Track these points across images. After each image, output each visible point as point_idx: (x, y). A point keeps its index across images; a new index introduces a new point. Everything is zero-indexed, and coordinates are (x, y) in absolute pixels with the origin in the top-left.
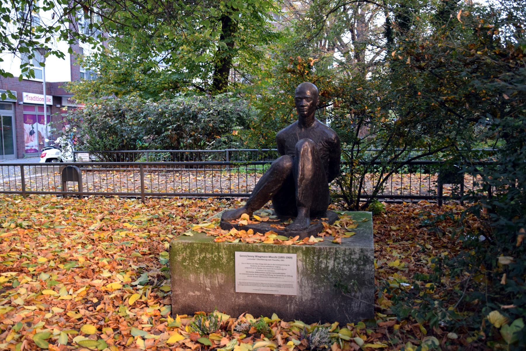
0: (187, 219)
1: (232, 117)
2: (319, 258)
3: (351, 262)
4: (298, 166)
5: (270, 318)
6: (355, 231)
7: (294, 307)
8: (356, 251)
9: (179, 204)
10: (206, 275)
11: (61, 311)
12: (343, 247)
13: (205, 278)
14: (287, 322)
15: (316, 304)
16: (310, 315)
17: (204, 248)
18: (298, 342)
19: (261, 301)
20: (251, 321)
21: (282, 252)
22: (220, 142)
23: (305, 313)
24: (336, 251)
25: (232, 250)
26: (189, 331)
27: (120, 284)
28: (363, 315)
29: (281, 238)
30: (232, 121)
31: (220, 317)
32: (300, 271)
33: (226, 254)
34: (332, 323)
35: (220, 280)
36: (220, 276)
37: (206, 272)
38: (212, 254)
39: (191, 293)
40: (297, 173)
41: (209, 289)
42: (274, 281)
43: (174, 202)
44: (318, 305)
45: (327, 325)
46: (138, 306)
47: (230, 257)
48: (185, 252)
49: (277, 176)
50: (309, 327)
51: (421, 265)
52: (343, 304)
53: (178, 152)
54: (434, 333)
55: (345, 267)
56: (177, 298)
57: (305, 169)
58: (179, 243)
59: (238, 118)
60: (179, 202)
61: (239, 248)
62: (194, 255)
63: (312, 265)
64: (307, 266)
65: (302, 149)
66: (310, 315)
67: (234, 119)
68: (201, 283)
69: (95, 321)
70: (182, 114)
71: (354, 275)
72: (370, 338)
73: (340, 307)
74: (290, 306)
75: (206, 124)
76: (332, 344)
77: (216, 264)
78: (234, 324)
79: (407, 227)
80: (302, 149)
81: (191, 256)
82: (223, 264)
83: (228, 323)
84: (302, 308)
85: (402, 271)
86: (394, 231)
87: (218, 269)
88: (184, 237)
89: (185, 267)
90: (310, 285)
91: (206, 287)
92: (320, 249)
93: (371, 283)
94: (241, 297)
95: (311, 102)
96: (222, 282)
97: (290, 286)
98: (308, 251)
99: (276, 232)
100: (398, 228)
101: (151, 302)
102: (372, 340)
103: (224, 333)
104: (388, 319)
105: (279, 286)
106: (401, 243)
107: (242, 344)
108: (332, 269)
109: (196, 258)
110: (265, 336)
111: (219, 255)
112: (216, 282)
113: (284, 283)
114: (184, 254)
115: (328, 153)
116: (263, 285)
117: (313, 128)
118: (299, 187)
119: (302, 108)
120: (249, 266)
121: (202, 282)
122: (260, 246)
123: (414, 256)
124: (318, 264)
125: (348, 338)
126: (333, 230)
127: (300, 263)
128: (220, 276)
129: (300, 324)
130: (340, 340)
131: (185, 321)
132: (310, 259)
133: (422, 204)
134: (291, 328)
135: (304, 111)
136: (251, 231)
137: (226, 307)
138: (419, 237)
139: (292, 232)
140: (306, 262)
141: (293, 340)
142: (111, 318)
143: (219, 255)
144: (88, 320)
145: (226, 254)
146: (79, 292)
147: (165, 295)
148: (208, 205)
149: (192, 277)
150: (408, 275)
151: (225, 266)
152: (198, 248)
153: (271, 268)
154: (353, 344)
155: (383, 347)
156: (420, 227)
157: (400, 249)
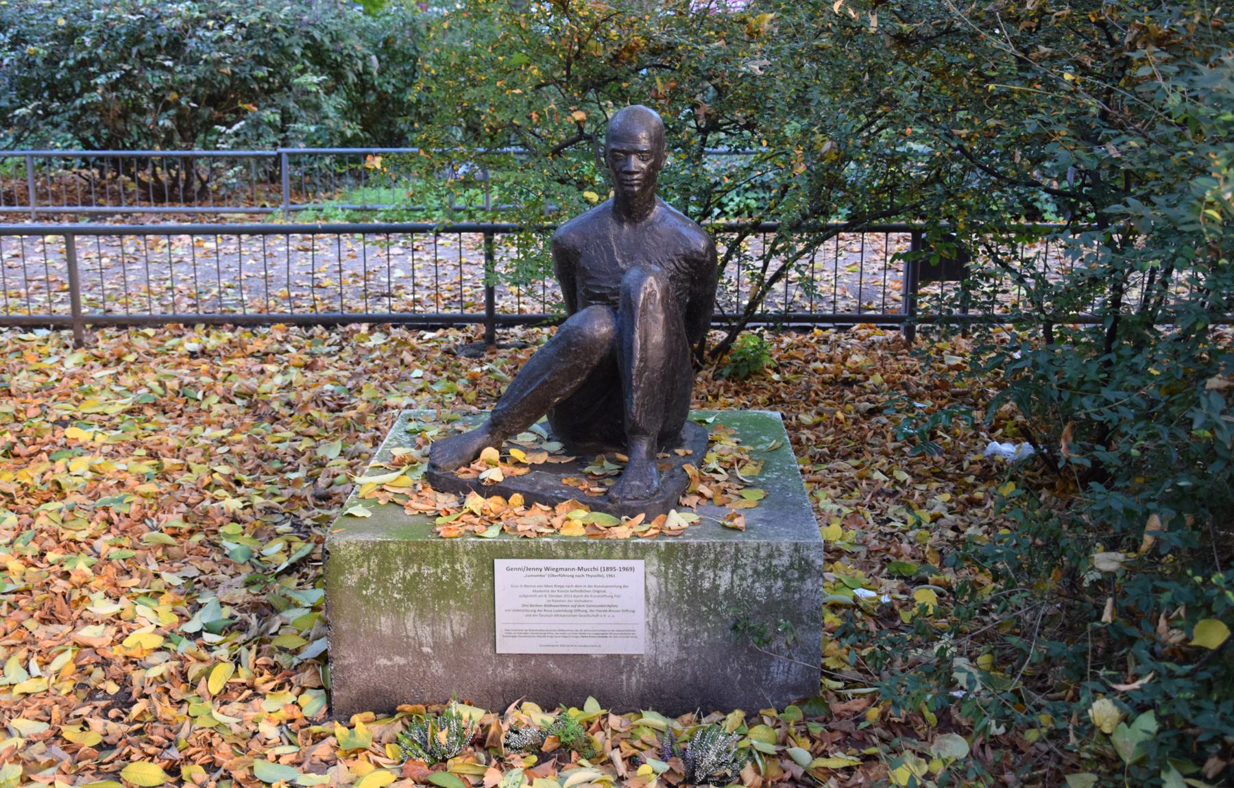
0: (239, 402)
1: (290, 45)
2: (696, 568)
3: (770, 573)
4: (632, 341)
5: (581, 708)
6: (763, 486)
7: (638, 681)
8: (783, 548)
9: (194, 346)
10: (421, 616)
11: (43, 728)
12: (753, 542)
13: (418, 623)
14: (621, 714)
15: (689, 670)
16: (681, 696)
17: (416, 554)
18: (663, 767)
19: (558, 671)
20: (543, 721)
21: (609, 556)
22: (257, 124)
23: (663, 692)
24: (738, 550)
25: (487, 557)
26: (395, 756)
27: (154, 632)
28: (795, 689)
29: (601, 519)
30: (292, 58)
31: (466, 716)
32: (652, 599)
33: (472, 566)
34: (726, 711)
35: (456, 627)
36: (456, 618)
37: (421, 610)
38: (437, 567)
39: (383, 662)
40: (631, 353)
41: (429, 650)
42: (588, 623)
43: (175, 341)
44: (694, 673)
45: (716, 716)
46: (235, 695)
47: (482, 571)
48: (366, 564)
49: (576, 359)
50: (676, 725)
51: (892, 534)
52: (750, 667)
53: (132, 157)
54: (954, 722)
55: (757, 585)
56: (346, 675)
57: (650, 346)
58: (349, 543)
59: (306, 47)
60: (189, 340)
61: (504, 552)
62: (389, 571)
63: (681, 584)
64: (669, 586)
65: (642, 296)
66: (681, 696)
67: (298, 51)
68: (408, 637)
69: (151, 750)
70: (135, 37)
71: (778, 603)
72: (818, 743)
73: (743, 676)
74: (629, 678)
75: (211, 67)
76: (742, 767)
77: (447, 590)
78: (501, 728)
79: (840, 415)
80: (642, 296)
81: (380, 574)
82: (463, 588)
83: (485, 728)
84: (656, 681)
85: (851, 554)
86: (808, 427)
87: (452, 602)
88: (350, 519)
89: (367, 600)
90: (675, 628)
91: (421, 645)
92: (700, 547)
93: (815, 620)
94: (511, 665)
95: (652, 161)
96: (461, 630)
97: (627, 634)
98: (673, 554)
99: (585, 503)
100: (818, 419)
101: (264, 683)
102: (823, 748)
103: (482, 756)
104: (850, 693)
105: (603, 635)
106: (831, 465)
107: (535, 781)
108: (726, 591)
109: (396, 578)
110: (581, 755)
111: (453, 568)
112: (448, 632)
113: (615, 628)
114: (364, 570)
115: (687, 285)
116: (563, 634)
117: (651, 224)
118: (638, 388)
119: (629, 177)
120: (529, 591)
121: (411, 634)
122: (557, 545)
123: (872, 507)
124: (695, 581)
125: (771, 749)
126: (713, 485)
127: (653, 581)
128: (456, 618)
129: (652, 718)
130: (757, 756)
131: (376, 729)
132: (676, 570)
133: (863, 333)
134: (634, 731)
135: (632, 186)
136: (517, 499)
137: (471, 689)
138: (873, 445)
139: (626, 502)
140: (666, 578)
141: (649, 760)
142: (193, 740)
143: (453, 568)
144: (134, 749)
145: (472, 566)
146: (54, 666)
147: (296, 661)
148: (276, 346)
149: (385, 624)
150: (866, 566)
151: (470, 593)
152: (399, 553)
153: (581, 591)
154: (787, 763)
155: (853, 764)
156: (872, 412)
157: (834, 488)
